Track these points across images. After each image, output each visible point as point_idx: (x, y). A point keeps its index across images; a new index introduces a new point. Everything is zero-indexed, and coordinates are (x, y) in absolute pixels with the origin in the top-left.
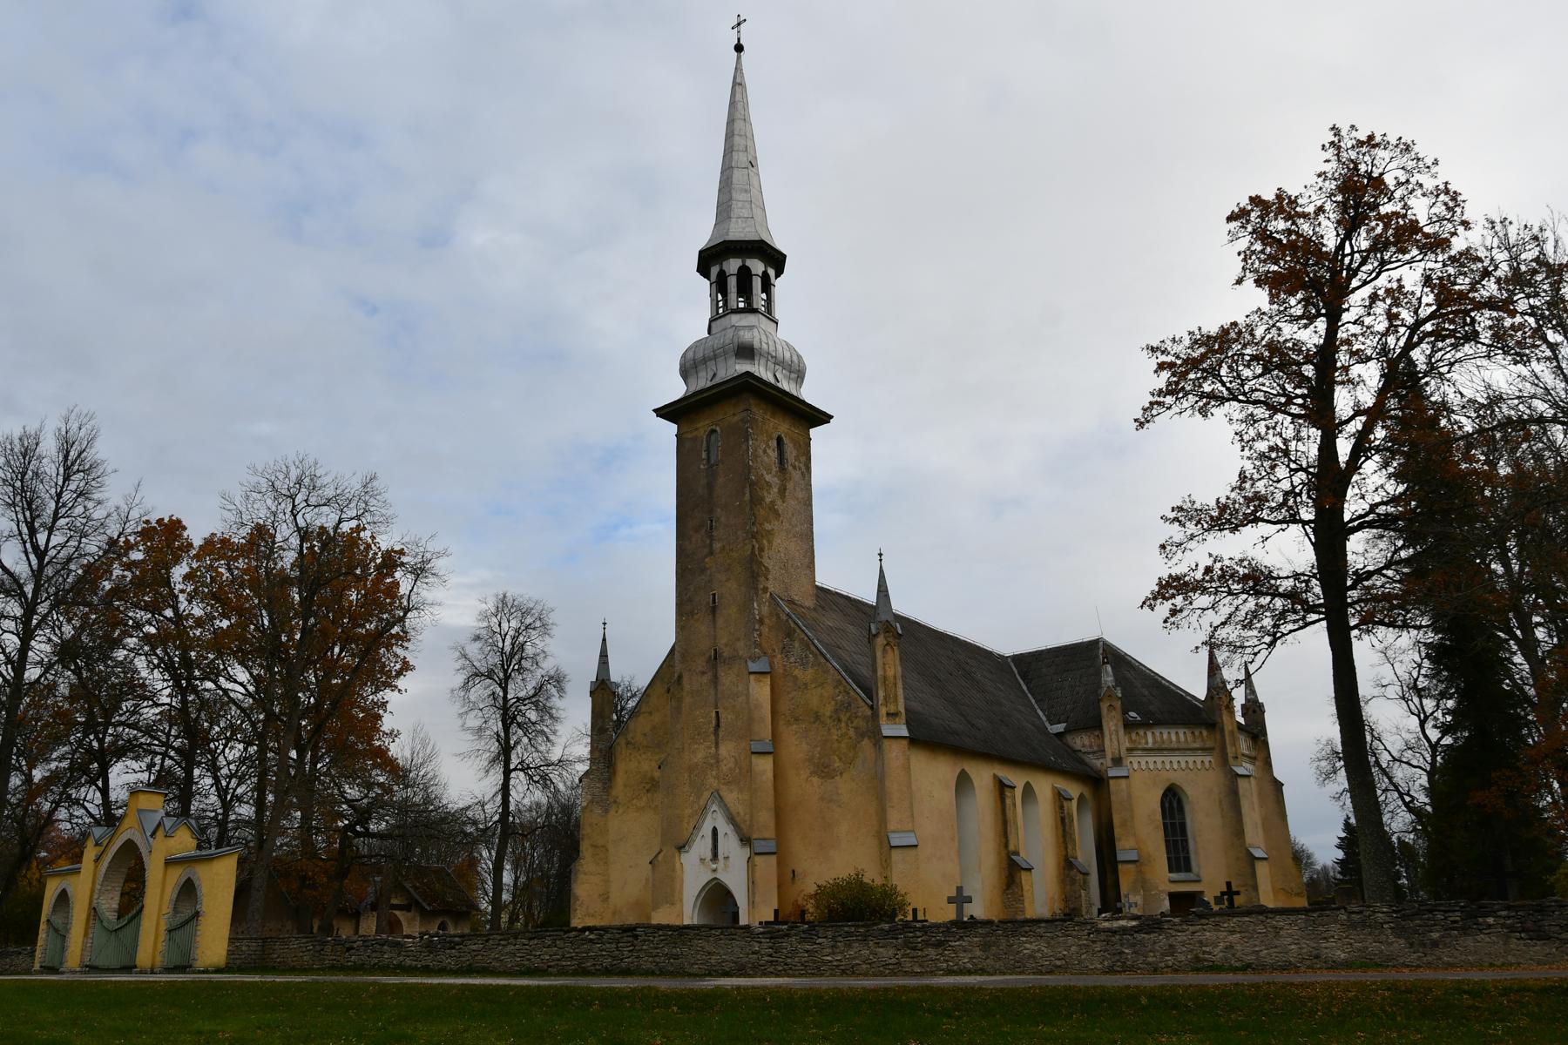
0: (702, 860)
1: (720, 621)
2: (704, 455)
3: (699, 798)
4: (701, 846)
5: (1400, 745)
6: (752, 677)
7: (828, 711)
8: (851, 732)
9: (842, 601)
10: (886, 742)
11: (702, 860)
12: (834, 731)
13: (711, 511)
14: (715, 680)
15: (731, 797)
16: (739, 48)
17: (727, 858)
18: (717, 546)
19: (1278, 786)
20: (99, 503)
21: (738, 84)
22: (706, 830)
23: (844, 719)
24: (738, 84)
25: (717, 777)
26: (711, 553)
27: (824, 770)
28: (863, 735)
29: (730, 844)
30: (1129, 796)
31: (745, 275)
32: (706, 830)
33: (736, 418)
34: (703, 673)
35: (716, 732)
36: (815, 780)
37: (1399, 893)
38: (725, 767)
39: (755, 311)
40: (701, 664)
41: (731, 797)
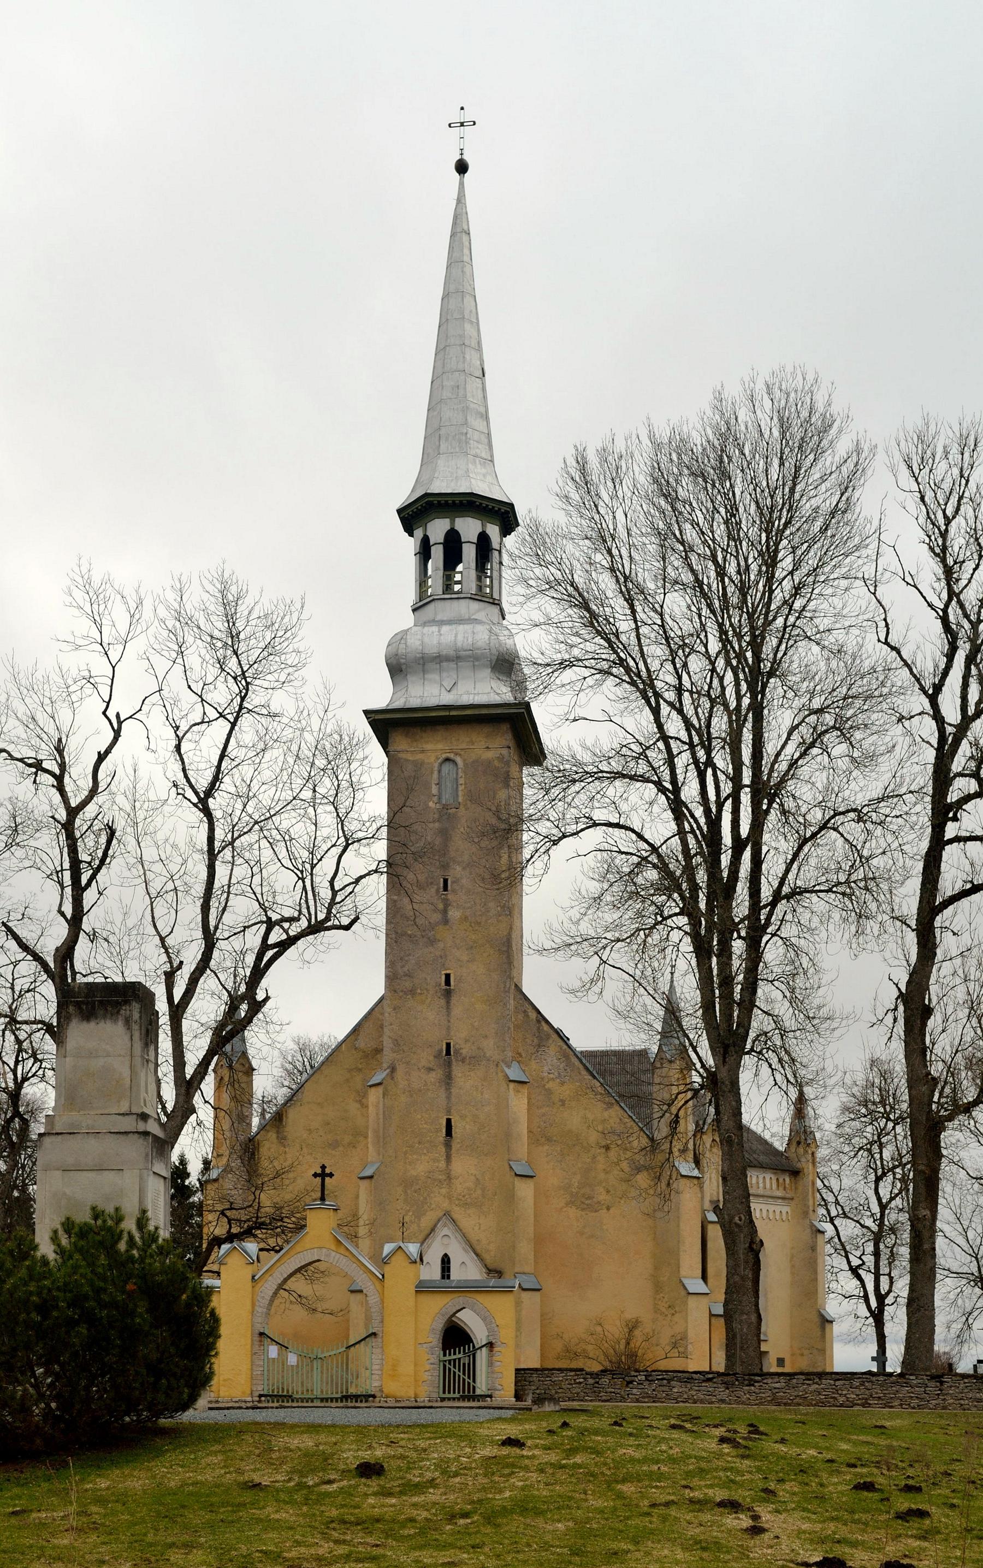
1: (457, 1011)
2: (434, 790)
6: (512, 1085)
8: (625, 1165)
9: (533, 1015)
12: (601, 1159)
13: (445, 867)
14: (448, 1080)
15: (469, 1221)
16: (462, 167)
18: (454, 914)
20: (212, 637)
21: (460, 231)
24: (460, 231)
25: (449, 1197)
26: (446, 921)
27: (583, 1201)
28: (639, 1170)
31: (453, 545)
34: (430, 1070)
35: (448, 1146)
36: (572, 1212)
37: (374, 1507)
39: (459, 596)
40: (426, 1057)
41: (469, 1221)
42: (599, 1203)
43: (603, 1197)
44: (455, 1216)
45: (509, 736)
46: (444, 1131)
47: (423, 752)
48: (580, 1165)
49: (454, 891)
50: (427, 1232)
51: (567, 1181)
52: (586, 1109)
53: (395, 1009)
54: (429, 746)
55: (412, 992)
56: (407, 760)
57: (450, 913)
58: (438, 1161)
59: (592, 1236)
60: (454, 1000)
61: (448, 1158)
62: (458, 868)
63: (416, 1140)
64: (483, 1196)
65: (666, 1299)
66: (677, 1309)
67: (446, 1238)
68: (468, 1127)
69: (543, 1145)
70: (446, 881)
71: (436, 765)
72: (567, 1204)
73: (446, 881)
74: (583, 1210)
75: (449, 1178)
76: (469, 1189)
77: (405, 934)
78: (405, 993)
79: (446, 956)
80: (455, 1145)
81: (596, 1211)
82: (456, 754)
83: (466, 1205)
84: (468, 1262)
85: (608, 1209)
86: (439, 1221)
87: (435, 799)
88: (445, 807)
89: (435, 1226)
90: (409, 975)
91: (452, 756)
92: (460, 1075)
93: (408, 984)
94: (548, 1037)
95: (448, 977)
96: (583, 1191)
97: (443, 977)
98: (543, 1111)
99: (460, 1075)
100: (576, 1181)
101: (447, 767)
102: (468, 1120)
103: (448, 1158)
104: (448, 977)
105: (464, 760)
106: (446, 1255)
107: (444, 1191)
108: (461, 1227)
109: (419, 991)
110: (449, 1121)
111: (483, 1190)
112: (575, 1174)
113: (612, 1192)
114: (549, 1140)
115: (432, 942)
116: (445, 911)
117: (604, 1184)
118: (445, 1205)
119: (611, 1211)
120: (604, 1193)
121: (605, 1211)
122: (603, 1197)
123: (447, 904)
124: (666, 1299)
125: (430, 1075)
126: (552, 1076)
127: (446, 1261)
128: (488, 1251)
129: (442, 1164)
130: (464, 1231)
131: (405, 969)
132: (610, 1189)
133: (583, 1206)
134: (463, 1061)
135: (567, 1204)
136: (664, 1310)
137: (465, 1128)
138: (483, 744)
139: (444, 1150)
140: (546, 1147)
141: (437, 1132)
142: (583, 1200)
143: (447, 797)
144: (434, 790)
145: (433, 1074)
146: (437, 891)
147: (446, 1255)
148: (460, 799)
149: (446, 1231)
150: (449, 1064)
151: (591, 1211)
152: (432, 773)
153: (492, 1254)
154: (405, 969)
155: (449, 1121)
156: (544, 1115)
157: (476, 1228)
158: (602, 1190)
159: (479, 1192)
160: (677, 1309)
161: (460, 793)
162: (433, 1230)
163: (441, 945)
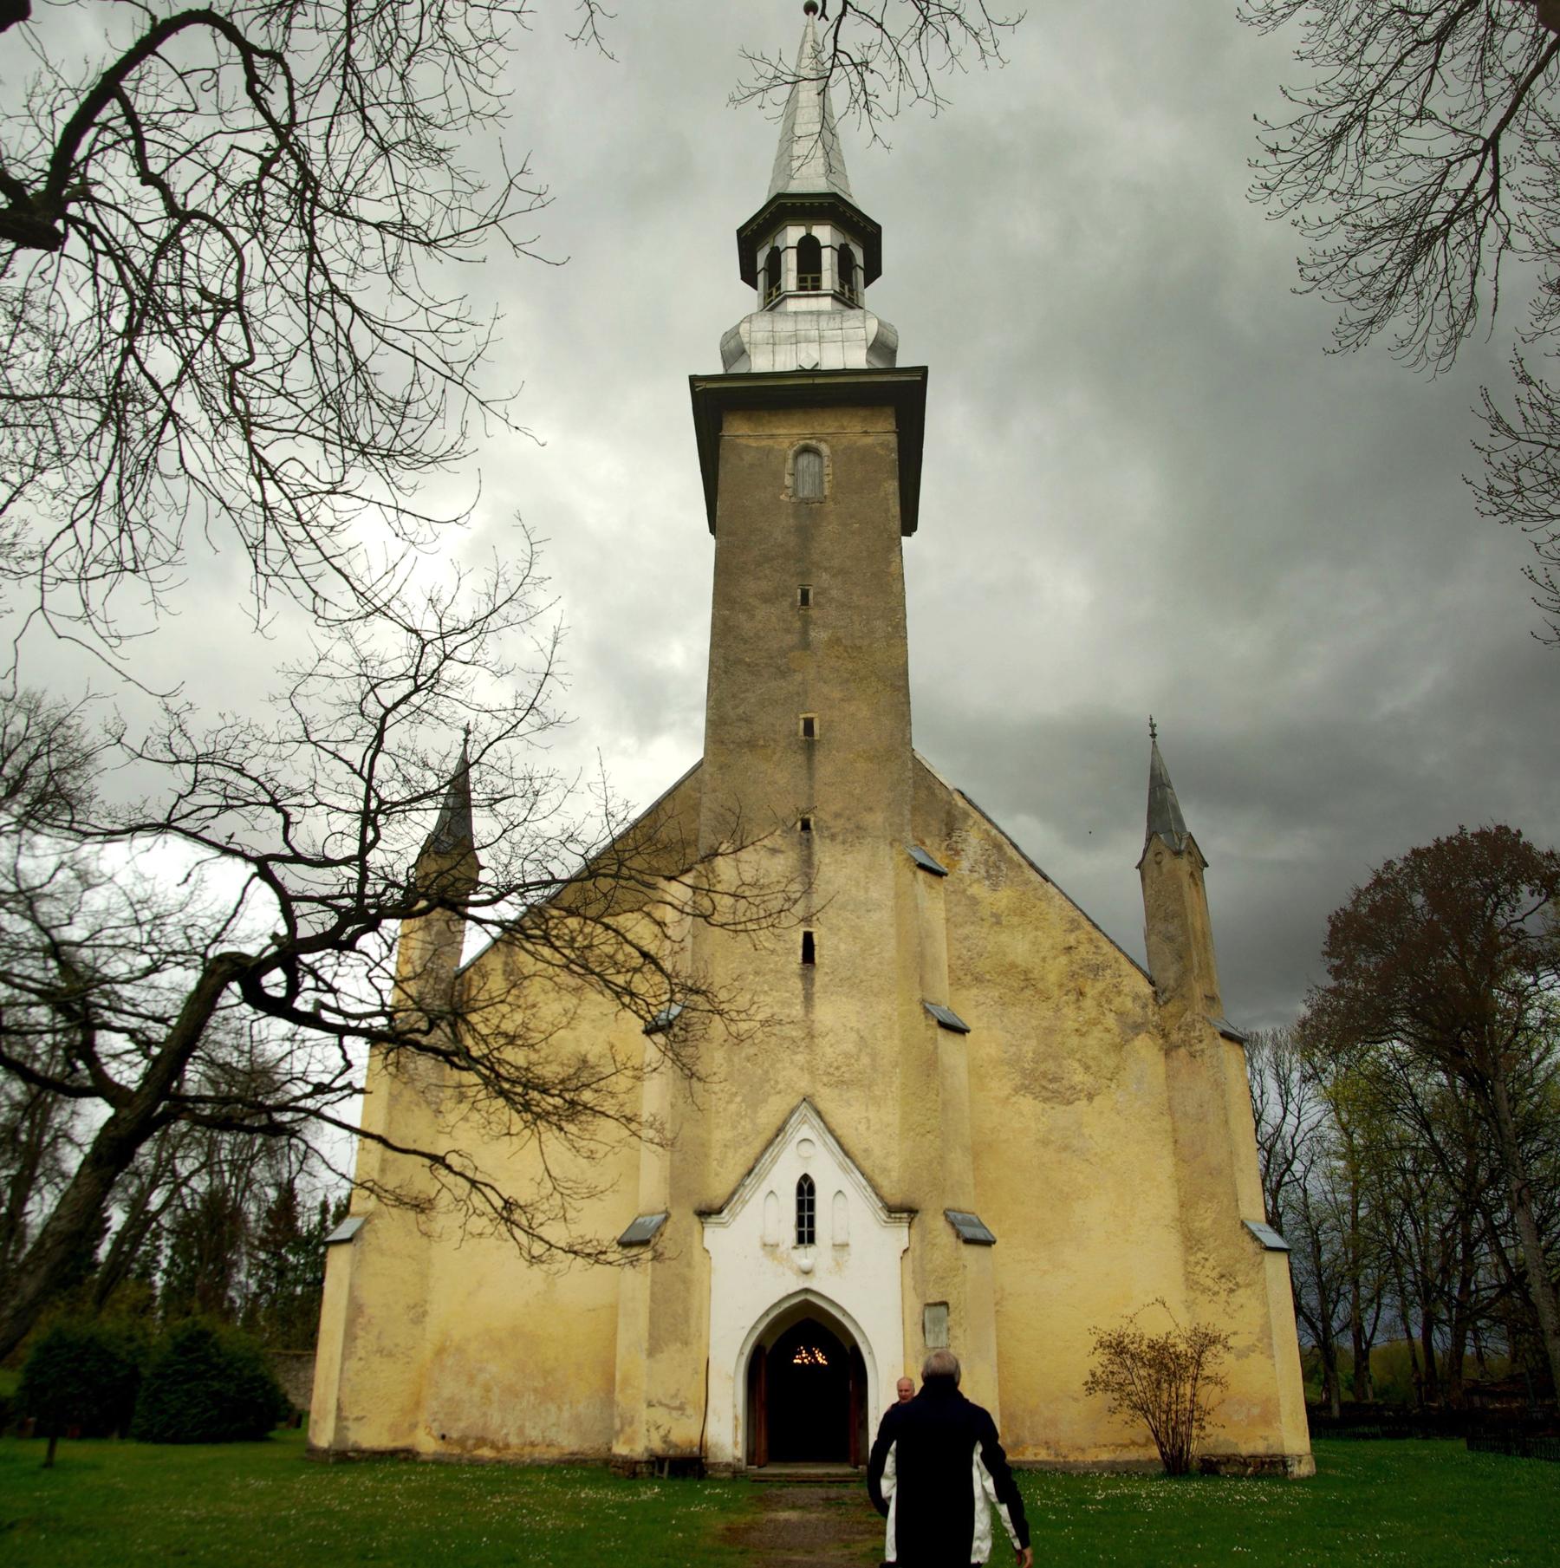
0: (770, 1248)
3: (754, 1104)
4: (769, 1209)
5: (446, 1220)
7: (1054, 971)
8: (1110, 1020)
10: (469, 923)
11: (770, 1248)
13: (805, 574)
17: (843, 1246)
18: (819, 635)
19: (713, 530)
22: (782, 1179)
23: (1091, 992)
25: (811, 1070)
26: (805, 645)
27: (1046, 1085)
28: (1137, 1028)
29: (846, 1210)
30: (269, 1440)
32: (782, 1179)
33: (869, 440)
36: (1027, 1104)
38: (828, 1050)
41: (848, 1113)
42: (1073, 1088)
43: (1079, 1077)
44: (821, 1106)
45: (891, 425)
46: (800, 952)
47: (772, 436)
48: (1034, 1023)
49: (817, 604)
50: (769, 1134)
51: (1013, 1049)
52: (1036, 929)
53: (721, 768)
54: (781, 431)
55: (751, 745)
56: (748, 447)
57: (813, 634)
58: (790, 1005)
59: (1066, 1148)
60: (819, 756)
61: (808, 999)
62: (825, 576)
63: (750, 969)
64: (874, 1069)
65: (1212, 1262)
66: (1240, 1279)
67: (806, 1145)
68: (842, 947)
69: (968, 987)
70: (805, 595)
71: (791, 453)
72: (1016, 1090)
73: (805, 595)
74: (1046, 1100)
75: (811, 1035)
76: (847, 1055)
77: (740, 661)
78: (739, 745)
79: (806, 692)
80: (820, 978)
81: (1070, 1103)
82: (820, 440)
83: (841, 1083)
84: (850, 1191)
85: (1090, 1097)
86: (792, 1112)
87: (790, 492)
88: (806, 501)
89: (785, 1122)
90: (746, 719)
91: (813, 442)
92: (827, 860)
93: (743, 733)
94: (966, 815)
95: (809, 724)
96: (1043, 1067)
97: (802, 723)
98: (966, 931)
99: (827, 860)
100: (1029, 1048)
101: (804, 460)
102: (842, 934)
103: (808, 999)
104: (809, 724)
105: (832, 447)
106: (805, 1178)
107: (800, 1059)
108: (833, 1125)
109: (761, 742)
110: (808, 937)
111: (874, 1057)
112: (1026, 1037)
113: (1094, 1069)
114: (978, 979)
115: (783, 673)
116: (805, 632)
117: (1078, 1056)
118: (804, 1084)
119: (1097, 1100)
120: (1081, 1070)
121: (1084, 1102)
122: (1079, 1077)
123: (807, 622)
124: (1212, 1262)
125: (776, 860)
126: (976, 875)
127: (806, 1190)
128: (884, 1170)
129: (797, 1011)
130: (839, 1132)
131: (740, 710)
132: (1091, 1063)
133: (1044, 1093)
134: (833, 837)
135: (1016, 1090)
136: (1209, 1282)
137: (837, 949)
138: (858, 429)
139: (800, 986)
140: (974, 991)
141: (788, 954)
142: (1044, 1083)
143: (806, 492)
144: (788, 481)
145: (780, 859)
146: (793, 605)
147: (805, 1178)
148: (826, 493)
149: (806, 1131)
150: (808, 844)
151: (1060, 1103)
152: (785, 460)
153: (895, 1175)
154: (740, 710)
155: (808, 937)
156: (967, 938)
157: (862, 1127)
158: (1076, 1065)
159: (865, 1060)
160: (1240, 1279)
161: (826, 485)
162: (780, 1130)
163: (798, 677)
